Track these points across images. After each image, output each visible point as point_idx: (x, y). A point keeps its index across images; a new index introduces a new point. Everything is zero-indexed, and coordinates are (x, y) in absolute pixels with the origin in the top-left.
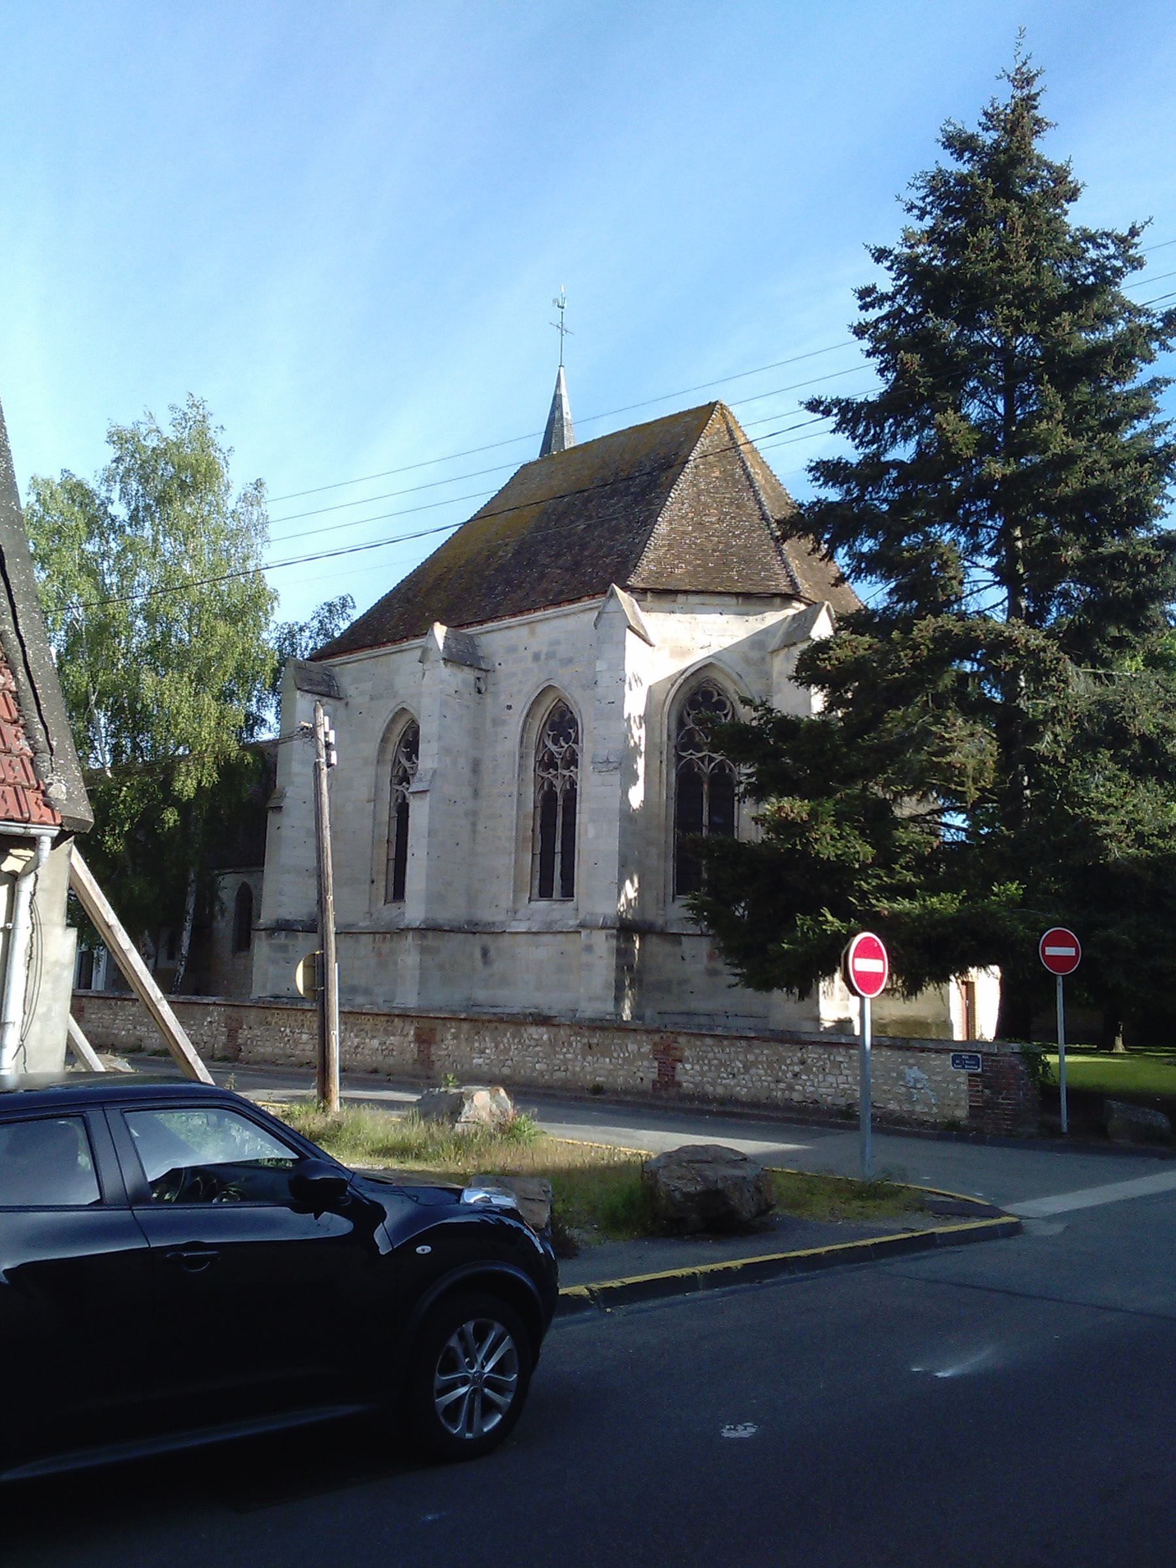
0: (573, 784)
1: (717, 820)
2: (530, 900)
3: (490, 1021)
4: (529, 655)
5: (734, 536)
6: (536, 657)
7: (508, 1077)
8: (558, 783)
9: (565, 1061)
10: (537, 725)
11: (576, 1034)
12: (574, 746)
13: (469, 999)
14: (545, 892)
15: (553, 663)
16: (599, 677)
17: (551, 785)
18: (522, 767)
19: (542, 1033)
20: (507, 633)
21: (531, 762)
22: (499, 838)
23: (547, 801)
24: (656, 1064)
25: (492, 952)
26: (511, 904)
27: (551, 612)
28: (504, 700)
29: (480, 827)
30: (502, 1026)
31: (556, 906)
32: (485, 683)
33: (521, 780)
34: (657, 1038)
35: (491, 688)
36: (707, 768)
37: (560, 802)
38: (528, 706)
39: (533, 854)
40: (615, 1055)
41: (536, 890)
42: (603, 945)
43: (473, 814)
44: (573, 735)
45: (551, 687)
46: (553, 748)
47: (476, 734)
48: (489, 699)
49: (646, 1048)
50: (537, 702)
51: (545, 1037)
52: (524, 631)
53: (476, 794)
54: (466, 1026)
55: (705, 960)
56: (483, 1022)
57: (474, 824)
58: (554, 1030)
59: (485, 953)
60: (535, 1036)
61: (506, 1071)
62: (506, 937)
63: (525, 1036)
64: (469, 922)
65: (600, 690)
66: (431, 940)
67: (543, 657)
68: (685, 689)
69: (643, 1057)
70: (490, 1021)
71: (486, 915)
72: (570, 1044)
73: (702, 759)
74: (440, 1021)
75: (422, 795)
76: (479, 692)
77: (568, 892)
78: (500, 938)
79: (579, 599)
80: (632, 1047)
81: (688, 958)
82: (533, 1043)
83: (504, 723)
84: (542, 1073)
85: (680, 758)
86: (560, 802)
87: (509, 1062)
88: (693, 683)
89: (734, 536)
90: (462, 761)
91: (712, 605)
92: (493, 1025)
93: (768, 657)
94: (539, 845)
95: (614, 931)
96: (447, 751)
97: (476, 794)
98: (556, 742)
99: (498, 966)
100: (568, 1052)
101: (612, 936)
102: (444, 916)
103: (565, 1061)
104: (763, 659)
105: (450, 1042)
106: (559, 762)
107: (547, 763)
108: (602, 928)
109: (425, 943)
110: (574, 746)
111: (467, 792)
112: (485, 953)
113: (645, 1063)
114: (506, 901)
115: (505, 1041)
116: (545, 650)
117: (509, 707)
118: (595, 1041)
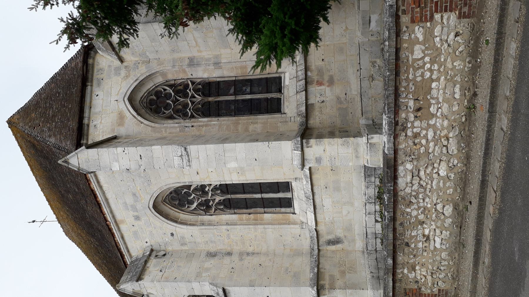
0: (216, 188)
1: (232, 91)
2: (294, 213)
3: (394, 230)
4: (136, 223)
5: (59, 97)
6: (137, 218)
7: (455, 208)
8: (218, 199)
9: (436, 140)
10: (183, 216)
11: (405, 129)
12: (192, 188)
13: (363, 252)
14: (288, 203)
15: (139, 206)
16: (123, 167)
17: (219, 203)
18: (210, 224)
19: (405, 169)
20: (126, 238)
21: (207, 218)
22: (256, 236)
23: (230, 205)
24: (437, 16)
25: (331, 237)
26: (297, 226)
27: (105, 210)
28: (168, 238)
29: (250, 250)
30: (400, 218)
31: (295, 194)
32: (160, 251)
33: (219, 224)
34: (405, 19)
35: (163, 248)
36: (198, 98)
37: (229, 196)
38: (169, 222)
39: (265, 213)
40: (428, 75)
41: (288, 210)
42: (316, 149)
43: (243, 255)
44: (185, 190)
45: (155, 207)
46: (195, 204)
47: (191, 256)
48: (170, 248)
49: (419, 33)
50: (167, 217)
51: (409, 166)
52: (123, 227)
53: (229, 254)
54: (400, 258)
55: (322, 87)
56: (395, 238)
57: (248, 254)
58: (401, 157)
59: (331, 242)
60: (409, 178)
61: (449, 210)
62: (321, 228)
63: (408, 190)
64: (312, 255)
65: (133, 166)
66: (326, 282)
67: (136, 214)
68: (147, 116)
69: (429, 35)
70: (394, 230)
71: (306, 242)
72: (416, 135)
73: (193, 103)
74: (398, 285)
75: (227, 291)
76: (164, 255)
77: (286, 187)
78: (321, 232)
79: (93, 191)
80: (418, 52)
81: (322, 99)
82: (416, 181)
83: (183, 238)
84: (451, 169)
85: (192, 117)
86: (229, 196)
87: (439, 207)
88: (143, 111)
89: (59, 97)
90: (207, 265)
91: (91, 102)
92: (399, 229)
93: (125, 64)
94: (259, 210)
95: (304, 141)
96: (198, 276)
97: (229, 254)
98: (191, 202)
99: (339, 233)
100: (426, 137)
101: (307, 143)
102: (308, 274)
103: (436, 140)
104: (126, 67)
105: (420, 273)
106: (204, 199)
107: (206, 207)
108: (302, 150)
109: (327, 286)
110: (192, 188)
111: (227, 260)
112: (331, 242)
113: (437, 31)
114: (296, 230)
115: (414, 213)
116: (131, 213)
117: (172, 235)
118: (411, 103)
